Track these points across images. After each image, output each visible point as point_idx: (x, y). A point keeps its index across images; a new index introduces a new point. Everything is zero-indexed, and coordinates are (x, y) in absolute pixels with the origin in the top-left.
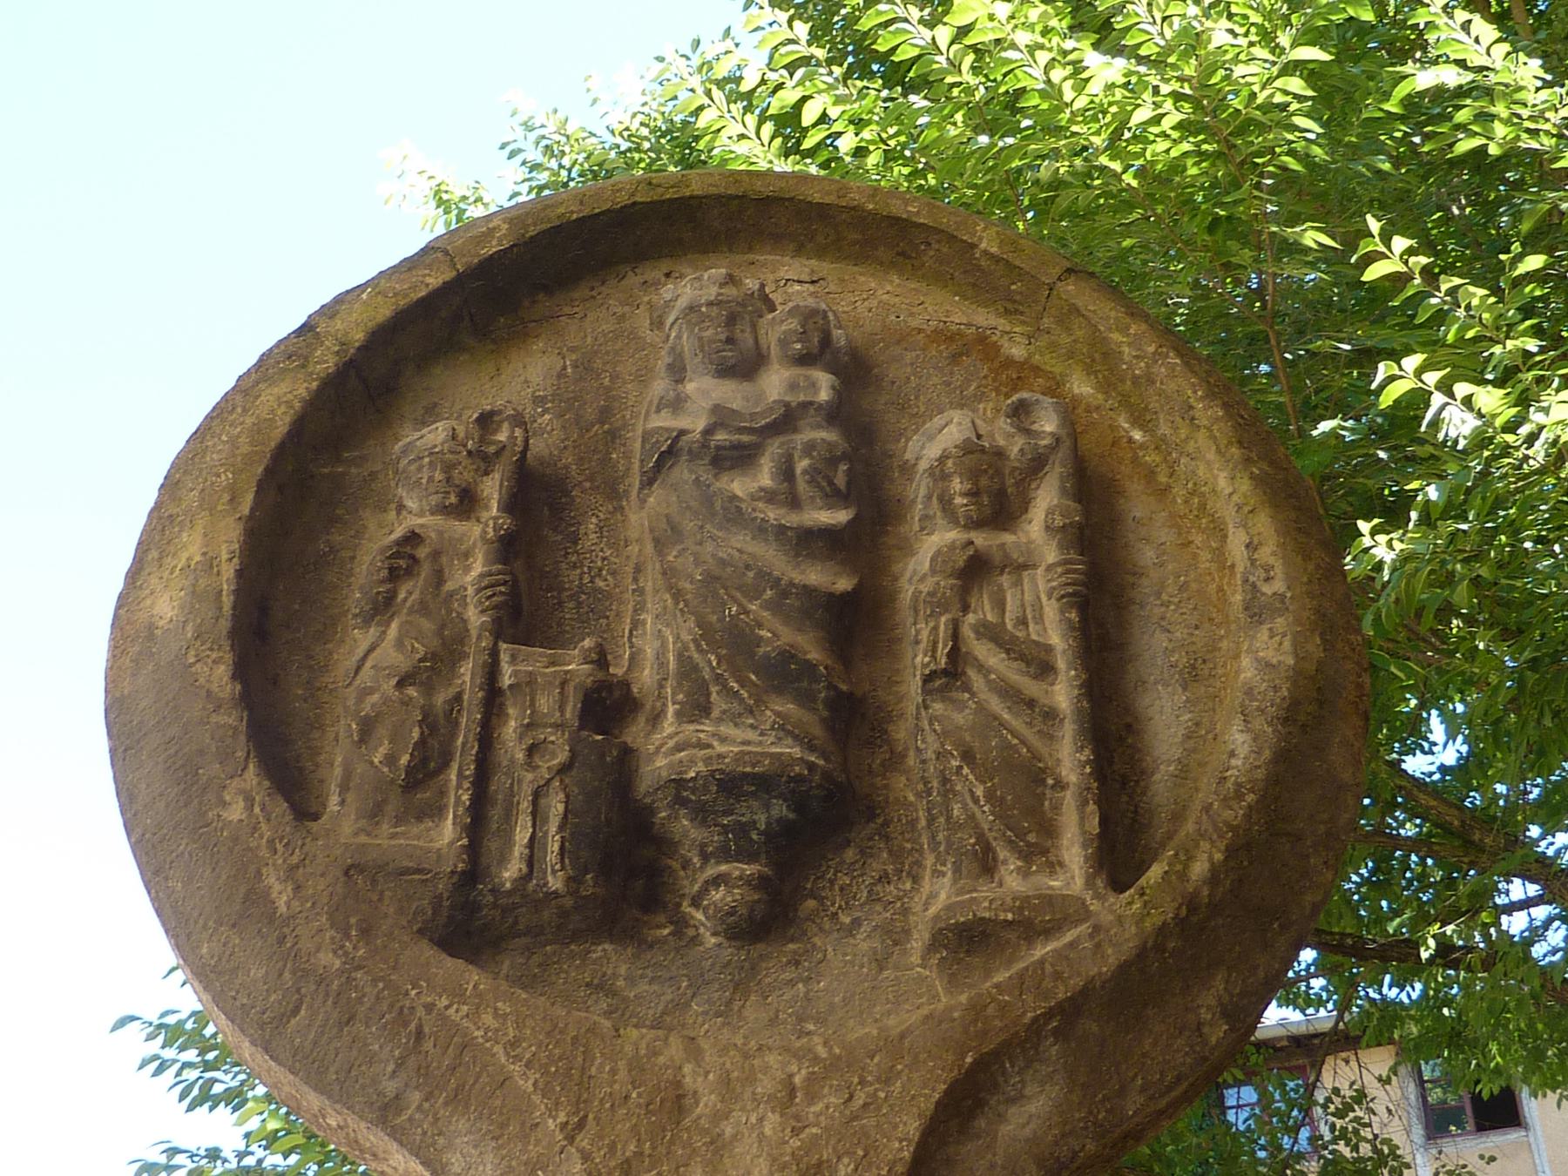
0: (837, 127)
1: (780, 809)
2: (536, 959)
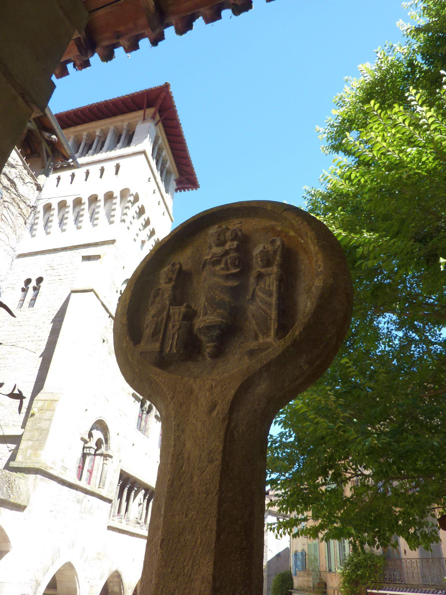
0: (359, 178)
1: (218, 332)
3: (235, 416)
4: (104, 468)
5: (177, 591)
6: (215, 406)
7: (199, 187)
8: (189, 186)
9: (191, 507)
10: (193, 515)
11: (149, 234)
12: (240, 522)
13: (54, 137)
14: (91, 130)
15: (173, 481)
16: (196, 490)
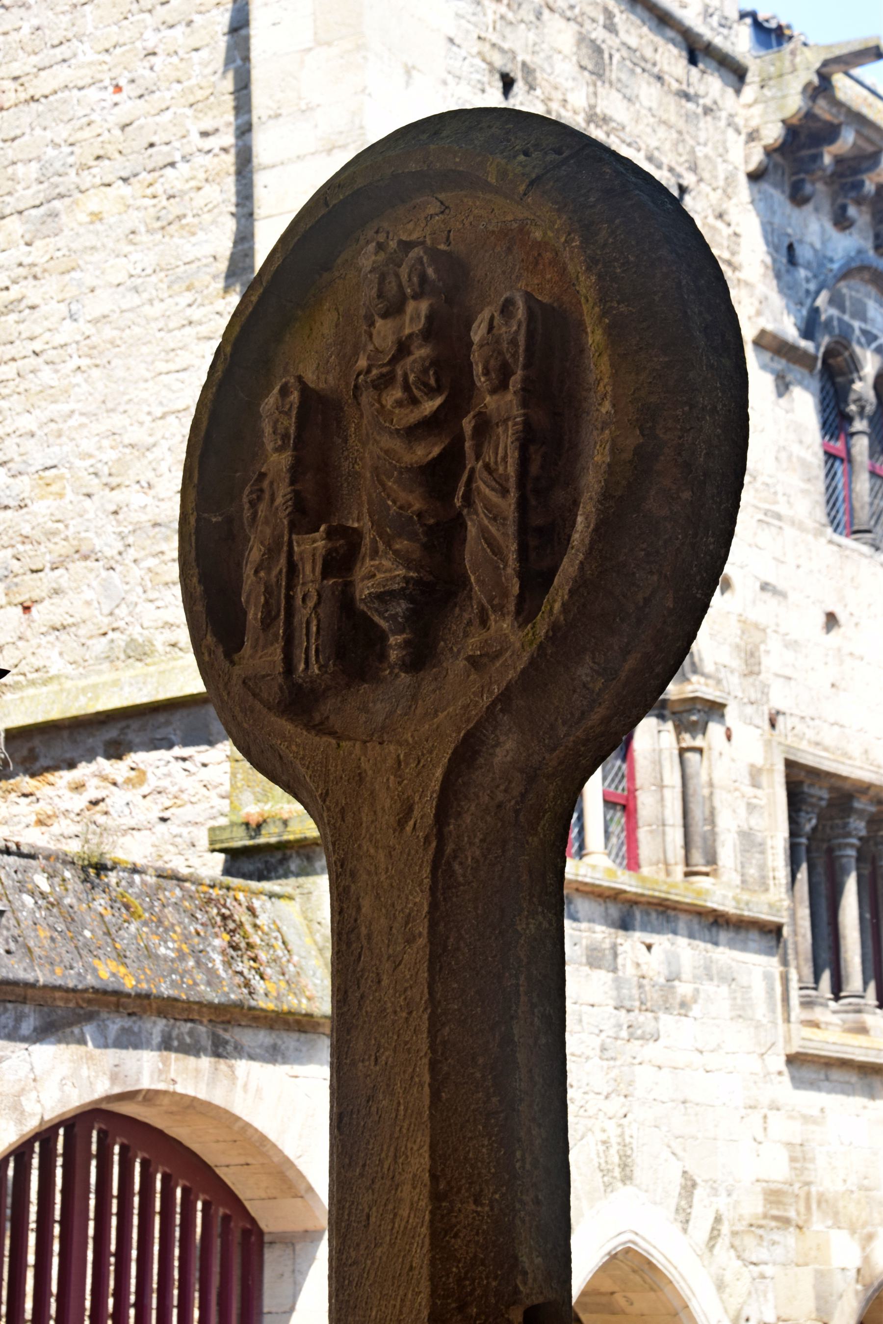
2: (339, 699)
3: (452, 827)
4: (690, 771)
5: (374, 1209)
6: (410, 809)
9: (383, 1041)
10: (387, 1058)
12: (481, 1061)
15: (346, 992)
16: (389, 1005)
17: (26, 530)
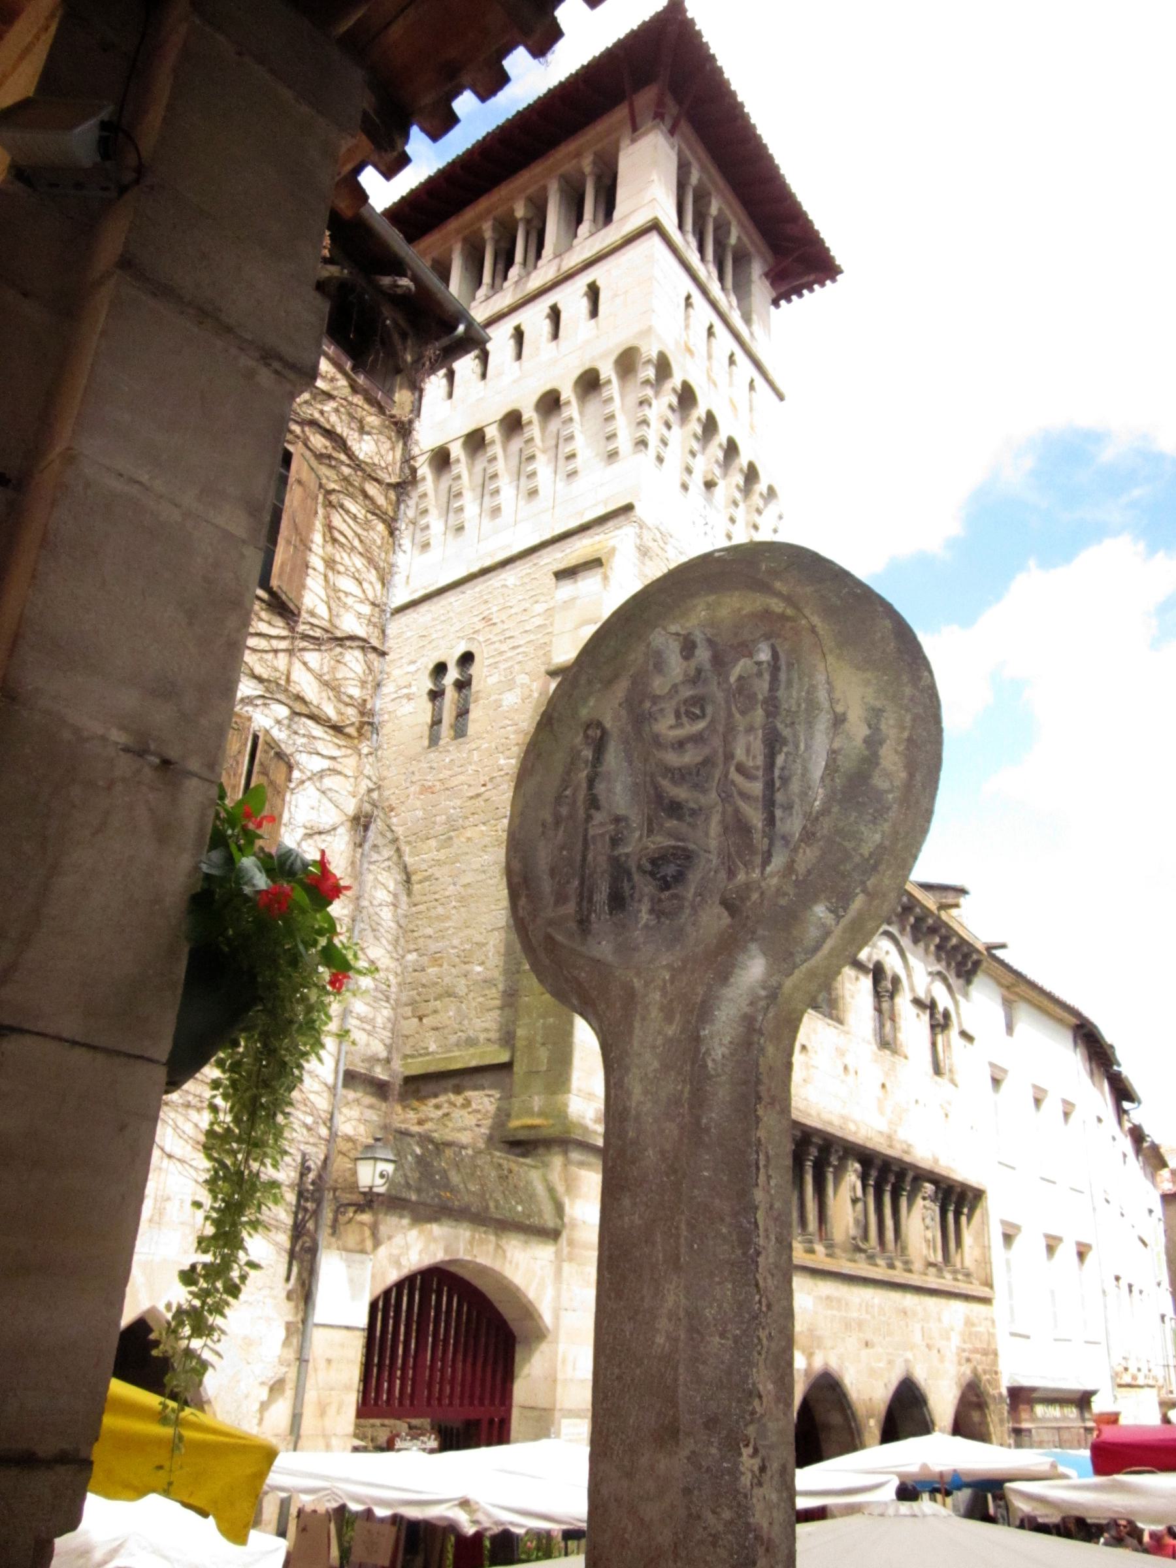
7: (841, 272)
8: (812, 277)
11: (720, 455)
13: (404, 282)
14: (500, 211)
17: (424, 981)
